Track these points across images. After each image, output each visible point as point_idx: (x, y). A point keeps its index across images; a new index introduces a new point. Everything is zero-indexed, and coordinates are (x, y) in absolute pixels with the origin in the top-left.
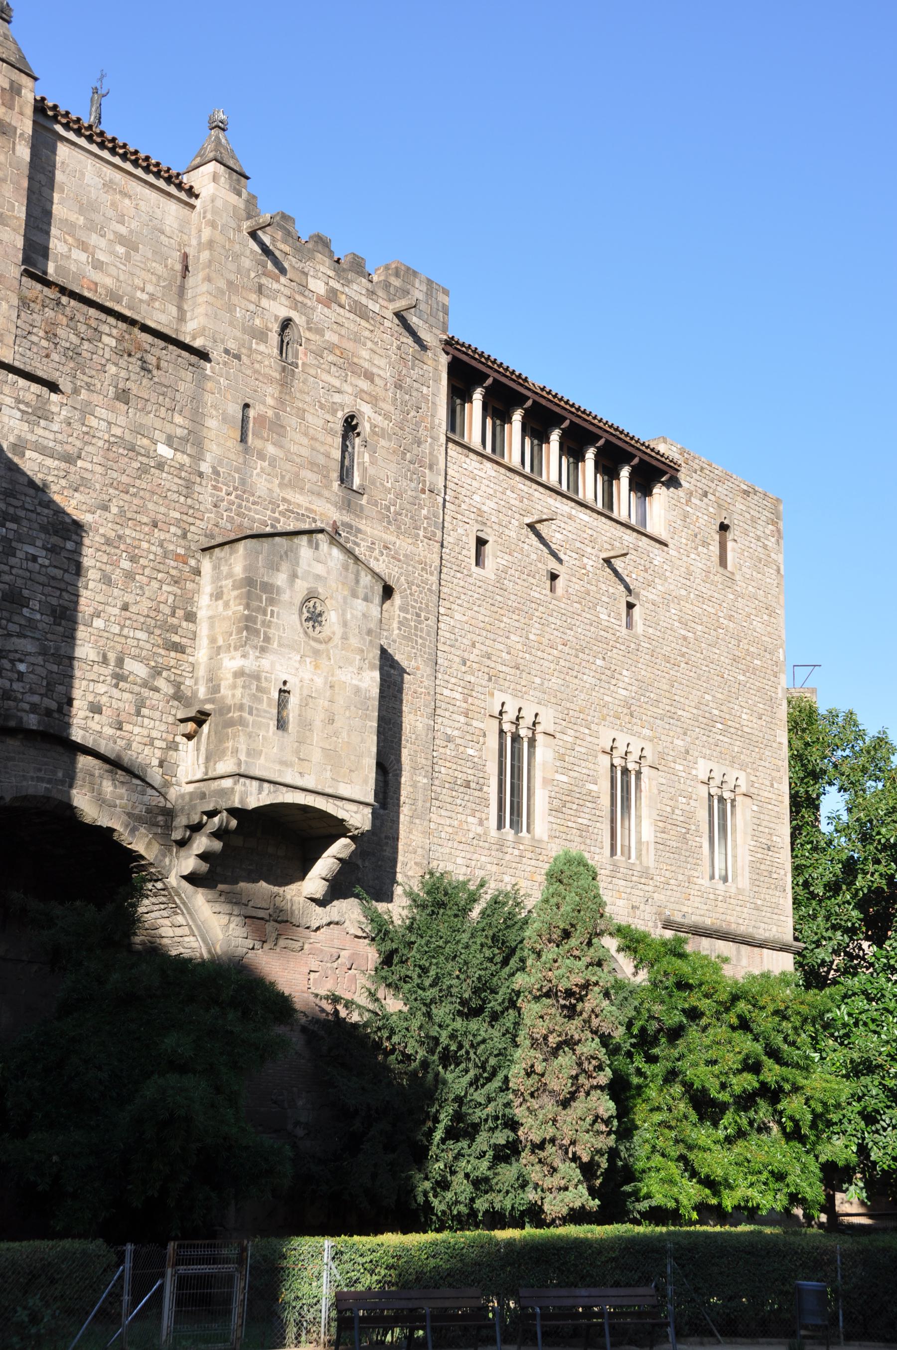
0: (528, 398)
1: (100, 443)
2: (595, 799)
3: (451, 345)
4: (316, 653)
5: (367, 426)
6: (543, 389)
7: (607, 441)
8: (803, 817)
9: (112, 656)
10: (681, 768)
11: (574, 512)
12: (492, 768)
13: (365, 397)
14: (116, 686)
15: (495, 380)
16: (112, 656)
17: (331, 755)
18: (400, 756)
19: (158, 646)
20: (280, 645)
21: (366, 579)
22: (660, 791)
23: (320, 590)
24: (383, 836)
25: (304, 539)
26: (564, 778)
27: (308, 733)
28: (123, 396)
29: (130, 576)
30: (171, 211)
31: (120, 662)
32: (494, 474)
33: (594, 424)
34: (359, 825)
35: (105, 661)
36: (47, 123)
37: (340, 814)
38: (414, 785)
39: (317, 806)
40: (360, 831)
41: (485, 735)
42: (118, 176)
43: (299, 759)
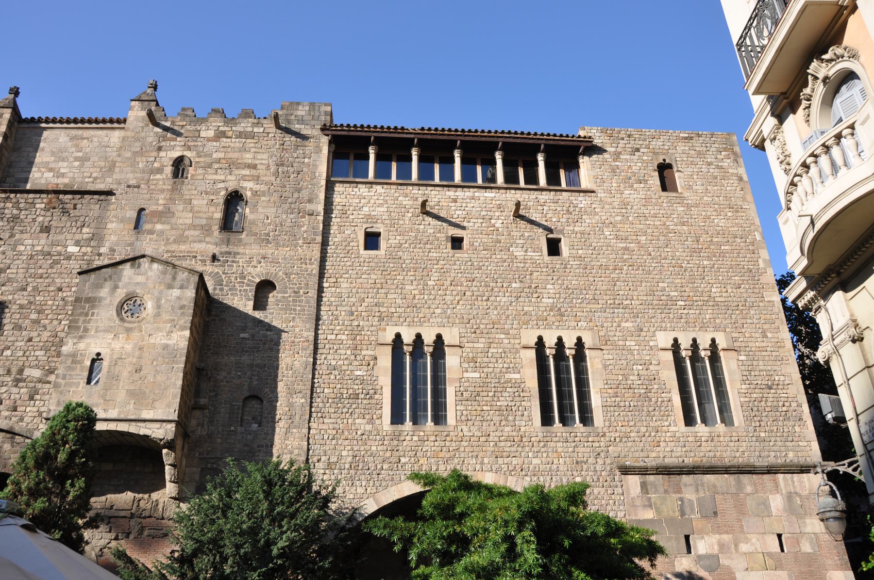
0: (414, 139)
1: (25, 258)
2: (519, 385)
3: (328, 130)
4: (128, 330)
5: (249, 194)
6: (423, 129)
7: (545, 145)
8: (234, 299)
9: (14, 370)
10: (634, 343)
11: (477, 194)
12: (385, 382)
13: (247, 178)
14: (16, 386)
15: (375, 137)
16: (14, 370)
17: (137, 396)
18: (276, 387)
19: (53, 357)
20: (97, 331)
21: (182, 276)
22: (605, 367)
23: (138, 291)
24: (255, 445)
25: (128, 265)
26: (477, 375)
27: (114, 382)
28: (46, 229)
29: (37, 322)
30: (115, 136)
31: (21, 371)
32: (383, 191)
33: (486, 136)
34: (162, 437)
35: (9, 372)
36: (36, 125)
37: (142, 432)
38: (291, 405)
39: (119, 429)
40: (165, 441)
41: (376, 358)
42: (80, 132)
43: (105, 400)
